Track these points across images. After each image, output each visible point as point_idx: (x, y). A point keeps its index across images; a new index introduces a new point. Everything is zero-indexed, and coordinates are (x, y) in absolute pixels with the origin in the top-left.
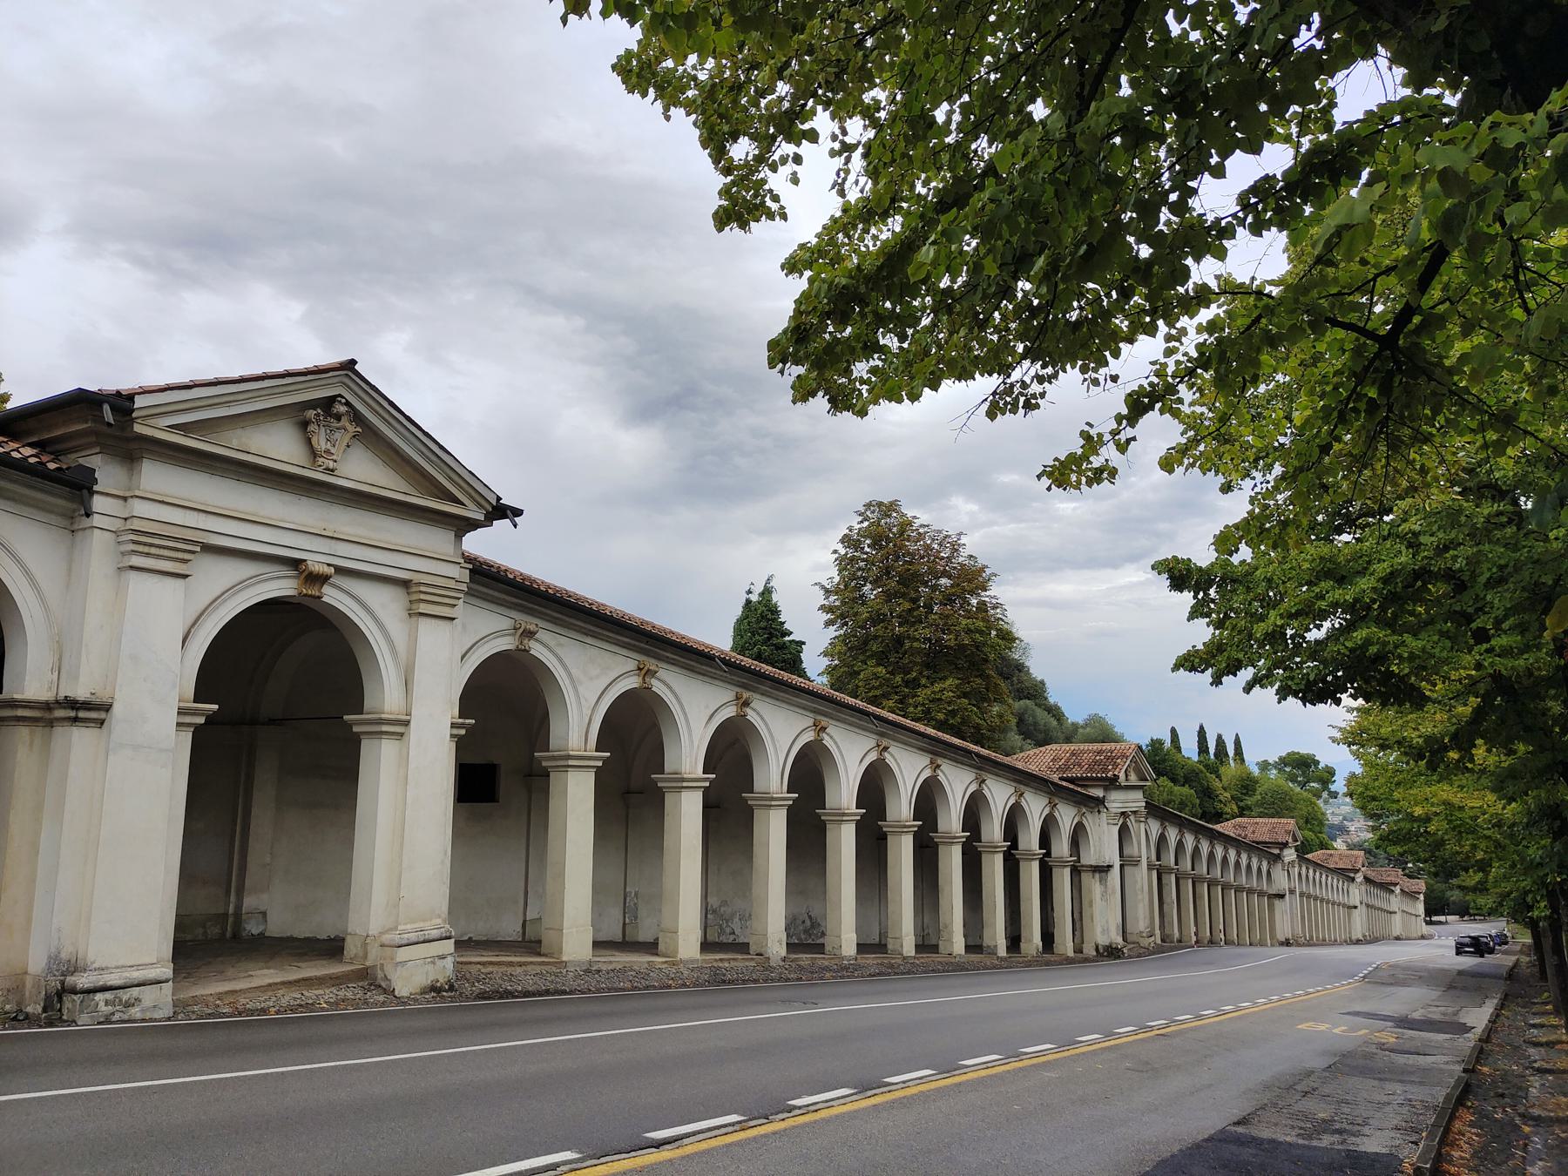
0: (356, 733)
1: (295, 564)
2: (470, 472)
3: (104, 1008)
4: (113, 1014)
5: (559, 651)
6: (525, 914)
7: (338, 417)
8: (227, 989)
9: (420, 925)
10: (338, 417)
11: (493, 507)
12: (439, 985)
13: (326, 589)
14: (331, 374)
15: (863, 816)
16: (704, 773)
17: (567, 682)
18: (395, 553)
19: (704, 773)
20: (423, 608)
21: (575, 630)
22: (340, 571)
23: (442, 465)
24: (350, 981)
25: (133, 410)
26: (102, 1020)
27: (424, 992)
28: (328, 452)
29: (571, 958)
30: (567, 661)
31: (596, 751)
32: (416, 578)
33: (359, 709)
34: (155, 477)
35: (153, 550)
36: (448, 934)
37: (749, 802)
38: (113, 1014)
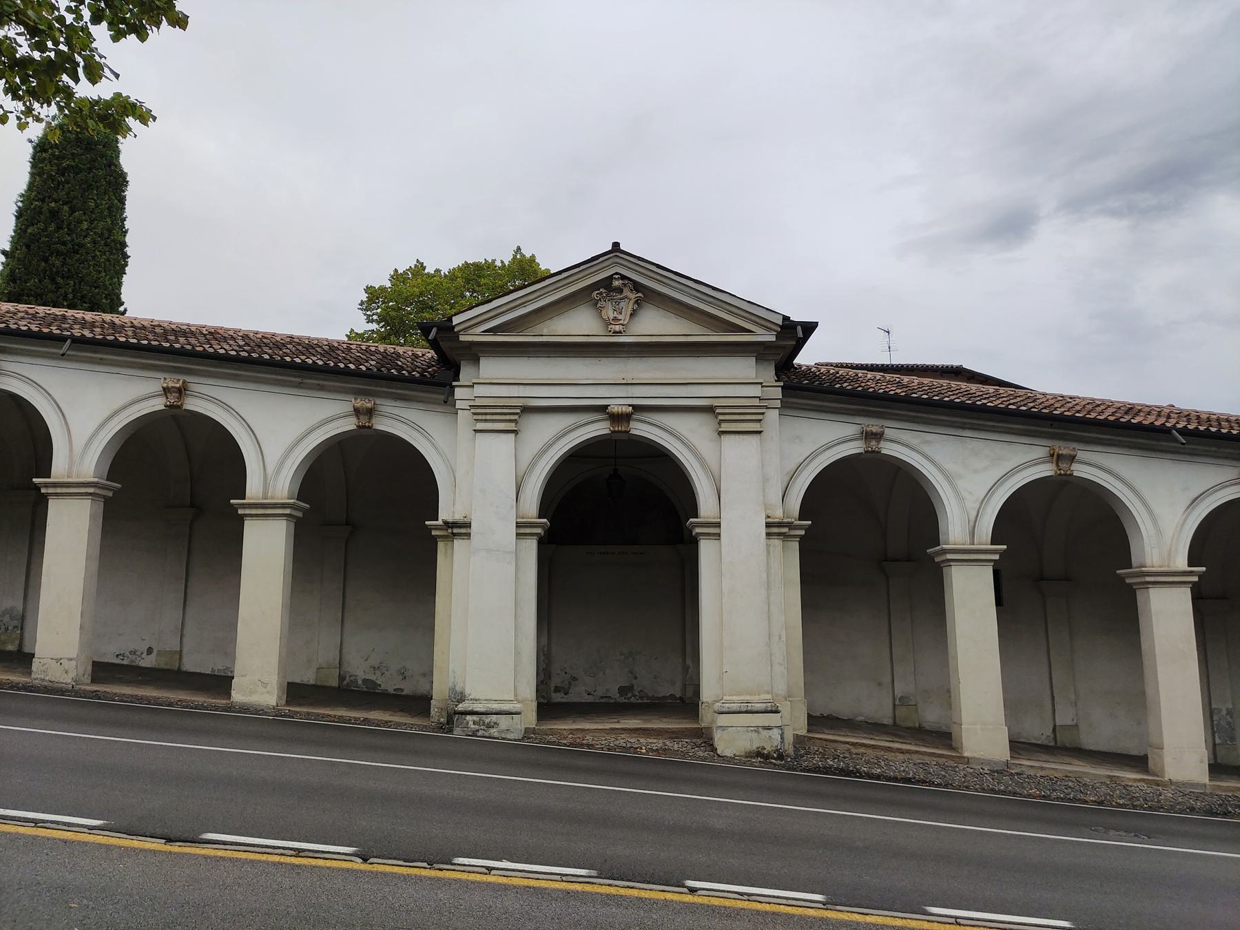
0: (937, 562)
1: (603, 409)
2: (749, 302)
3: (473, 726)
4: (478, 731)
5: (927, 449)
6: (1054, 719)
7: (620, 291)
8: (595, 727)
9: (748, 698)
10: (620, 291)
11: (781, 327)
12: (765, 752)
13: (633, 424)
14: (601, 259)
15: (1002, 554)
16: (1189, 566)
17: (940, 477)
18: (690, 386)
19: (1189, 566)
20: (725, 427)
21: (969, 429)
22: (637, 408)
23: (720, 303)
24: (685, 737)
25: (454, 327)
26: (470, 734)
27: (750, 755)
28: (615, 319)
29: (976, 755)
30: (937, 458)
31: (991, 544)
32: (716, 403)
33: (1129, 565)
34: (491, 368)
35: (488, 417)
36: (774, 709)
37: (937, 560)
38: (478, 731)
